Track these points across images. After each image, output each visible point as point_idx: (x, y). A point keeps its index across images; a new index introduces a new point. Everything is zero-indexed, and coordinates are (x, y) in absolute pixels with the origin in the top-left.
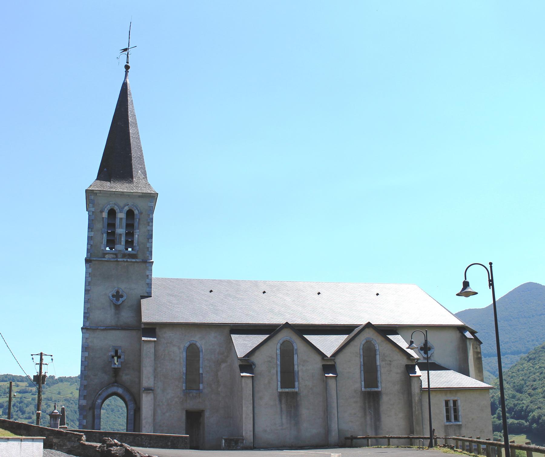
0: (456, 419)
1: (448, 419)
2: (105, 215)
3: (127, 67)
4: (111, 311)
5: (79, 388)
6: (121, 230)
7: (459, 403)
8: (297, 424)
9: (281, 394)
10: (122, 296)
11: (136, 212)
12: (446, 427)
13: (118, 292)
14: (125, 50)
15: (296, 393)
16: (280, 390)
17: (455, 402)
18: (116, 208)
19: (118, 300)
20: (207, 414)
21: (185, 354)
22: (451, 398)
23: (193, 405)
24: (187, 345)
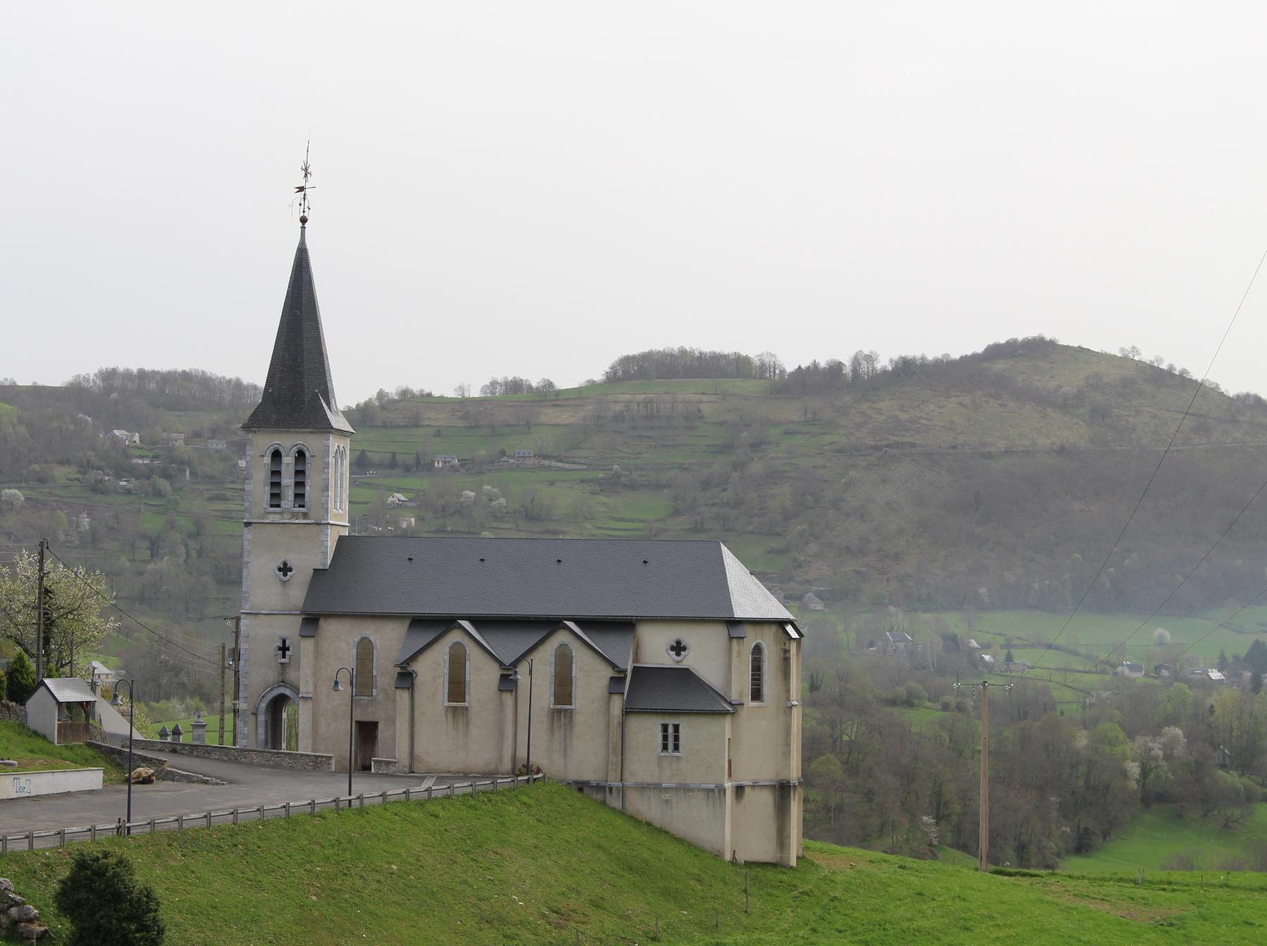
0: (676, 748)
1: (665, 747)
2: (267, 460)
3: (304, 220)
4: (277, 589)
5: (242, 819)
6: (288, 480)
7: (681, 729)
8: (636, 788)
9: (447, 708)
10: (290, 570)
11: (307, 454)
12: (660, 758)
13: (285, 564)
14: (301, 189)
15: (467, 708)
16: (447, 704)
17: (676, 728)
18: (281, 449)
19: (285, 575)
20: (381, 726)
21: (355, 651)
22: (671, 721)
23: (361, 716)
24: (357, 639)
